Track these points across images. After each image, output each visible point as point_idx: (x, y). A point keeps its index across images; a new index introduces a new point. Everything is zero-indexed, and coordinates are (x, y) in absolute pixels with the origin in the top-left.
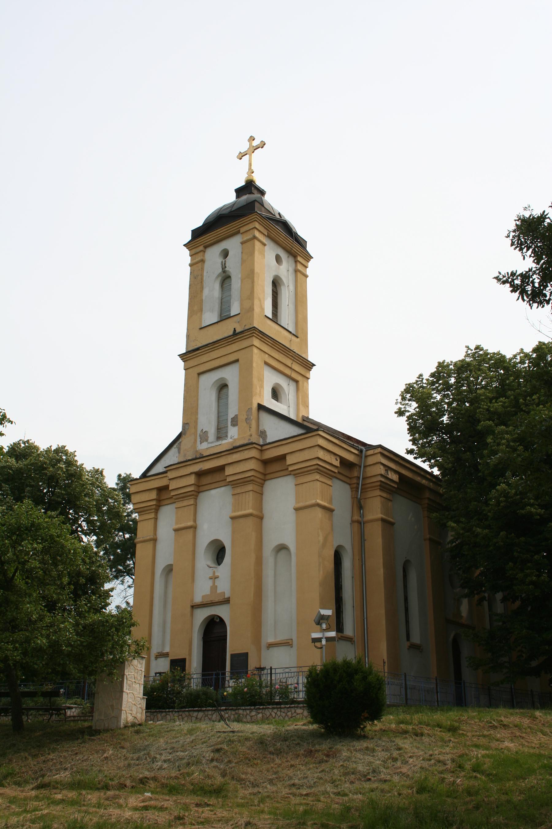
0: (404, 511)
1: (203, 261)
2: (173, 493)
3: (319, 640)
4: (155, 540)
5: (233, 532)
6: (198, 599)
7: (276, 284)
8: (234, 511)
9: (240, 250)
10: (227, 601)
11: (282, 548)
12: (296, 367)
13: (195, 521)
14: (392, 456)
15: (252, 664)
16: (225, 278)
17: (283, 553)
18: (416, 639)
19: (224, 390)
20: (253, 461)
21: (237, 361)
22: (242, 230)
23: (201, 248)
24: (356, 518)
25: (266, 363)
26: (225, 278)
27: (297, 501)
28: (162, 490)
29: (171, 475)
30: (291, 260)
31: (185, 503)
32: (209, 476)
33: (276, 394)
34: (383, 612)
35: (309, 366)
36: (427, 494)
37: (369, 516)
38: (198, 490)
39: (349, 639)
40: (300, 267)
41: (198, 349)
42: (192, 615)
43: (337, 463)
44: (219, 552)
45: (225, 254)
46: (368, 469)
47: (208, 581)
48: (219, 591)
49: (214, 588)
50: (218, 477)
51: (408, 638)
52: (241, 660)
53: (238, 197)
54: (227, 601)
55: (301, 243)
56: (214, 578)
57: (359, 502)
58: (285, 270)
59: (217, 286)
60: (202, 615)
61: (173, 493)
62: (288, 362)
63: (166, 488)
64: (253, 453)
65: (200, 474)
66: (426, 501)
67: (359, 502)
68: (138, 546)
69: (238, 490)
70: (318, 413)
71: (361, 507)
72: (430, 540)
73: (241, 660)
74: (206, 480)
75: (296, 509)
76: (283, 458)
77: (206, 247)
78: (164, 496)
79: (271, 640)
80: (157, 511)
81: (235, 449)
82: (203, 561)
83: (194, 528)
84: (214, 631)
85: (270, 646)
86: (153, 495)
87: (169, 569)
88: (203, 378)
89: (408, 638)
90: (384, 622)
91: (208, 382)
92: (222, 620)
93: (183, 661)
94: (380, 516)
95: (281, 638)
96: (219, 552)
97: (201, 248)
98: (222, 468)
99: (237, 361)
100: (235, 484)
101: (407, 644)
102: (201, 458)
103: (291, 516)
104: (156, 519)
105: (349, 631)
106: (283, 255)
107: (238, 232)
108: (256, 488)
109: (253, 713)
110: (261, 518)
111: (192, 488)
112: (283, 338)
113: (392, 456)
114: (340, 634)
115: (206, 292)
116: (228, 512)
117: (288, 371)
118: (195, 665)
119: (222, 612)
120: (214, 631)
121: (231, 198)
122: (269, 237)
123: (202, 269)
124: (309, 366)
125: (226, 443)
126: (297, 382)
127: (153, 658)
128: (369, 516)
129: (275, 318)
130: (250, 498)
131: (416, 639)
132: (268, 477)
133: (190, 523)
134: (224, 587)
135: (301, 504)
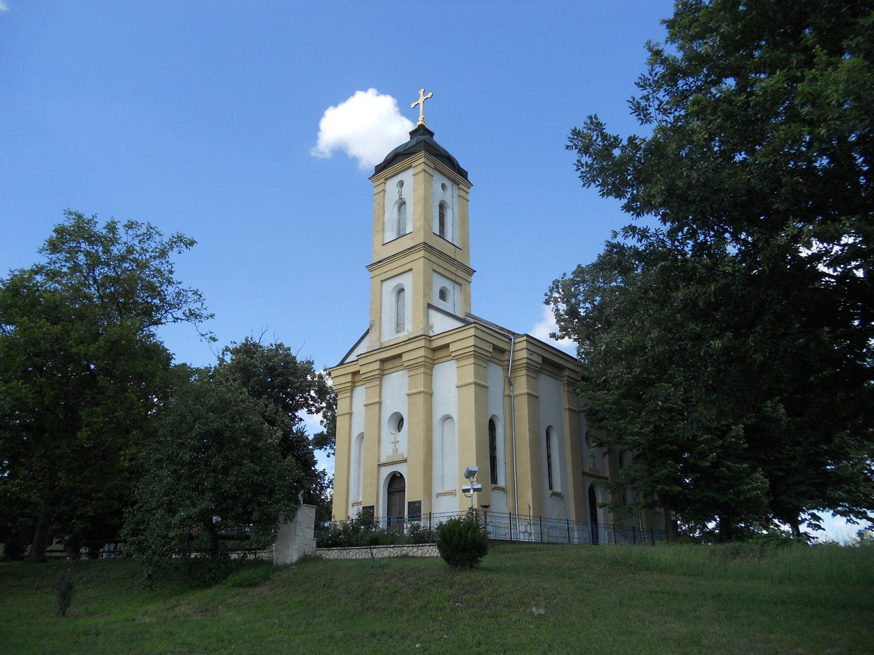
0: (553, 391)
1: (384, 191)
2: (363, 377)
3: (468, 490)
4: (351, 414)
5: (410, 405)
6: (383, 460)
7: (442, 206)
8: (410, 389)
9: (412, 181)
10: (405, 461)
11: (448, 418)
12: (460, 273)
13: (380, 397)
14: (540, 345)
15: (424, 510)
16: (402, 204)
17: (448, 423)
18: (557, 488)
19: (402, 294)
20: (423, 349)
21: (411, 269)
22: (414, 165)
23: (383, 180)
24: (507, 393)
25: (434, 270)
26: (402, 204)
27: (459, 381)
28: (355, 374)
29: (361, 362)
30: (455, 187)
31: (373, 384)
32: (390, 361)
33: (443, 295)
34: (529, 467)
35: (471, 272)
36: (566, 373)
37: (518, 391)
38: (382, 375)
39: (502, 489)
40: (462, 193)
41: (380, 261)
42: (378, 472)
43: (491, 350)
44: (399, 422)
45: (401, 184)
46: (517, 353)
47: (396, 446)
48: (399, 452)
49: (396, 450)
50: (397, 363)
51: (551, 488)
52: (415, 509)
53: (411, 138)
54: (405, 461)
55: (463, 174)
56: (396, 442)
57: (509, 379)
58: (450, 195)
59: (396, 210)
60: (386, 472)
61: (363, 377)
62: (453, 269)
63: (358, 372)
64: (422, 343)
65: (383, 361)
66: (566, 378)
67: (509, 379)
68: (338, 419)
69: (413, 373)
70: (477, 311)
71: (511, 384)
72: (570, 409)
73: (415, 509)
74: (388, 365)
75: (458, 387)
76: (447, 346)
77: (386, 180)
78: (357, 378)
79: (439, 491)
80: (352, 390)
81: (410, 340)
82: (387, 430)
83: (380, 403)
84: (396, 483)
85: (438, 495)
86: (349, 378)
87: (361, 436)
88: (385, 284)
89: (551, 488)
90: (530, 475)
91: (389, 287)
92: (401, 475)
93: (372, 507)
94: (526, 391)
95: (447, 489)
96: (399, 422)
97: (383, 180)
98: (400, 356)
99: (411, 269)
100: (409, 368)
101: (551, 492)
102: (382, 349)
103: (454, 392)
104: (351, 397)
105: (501, 482)
106: (448, 183)
107: (411, 167)
108: (428, 371)
109: (415, 550)
110: (432, 395)
111: (377, 372)
112: (449, 251)
113: (540, 345)
114: (494, 485)
115: (387, 215)
116: (406, 390)
117: (453, 277)
118: (381, 513)
119: (402, 469)
120: (396, 483)
121: (407, 138)
122: (435, 169)
123: (384, 197)
124: (471, 272)
125: (403, 336)
126: (460, 285)
127: (350, 506)
128: (518, 391)
129: (442, 235)
130: (421, 379)
131: (557, 488)
132: (436, 362)
133: (377, 400)
134: (403, 450)
135: (461, 383)
